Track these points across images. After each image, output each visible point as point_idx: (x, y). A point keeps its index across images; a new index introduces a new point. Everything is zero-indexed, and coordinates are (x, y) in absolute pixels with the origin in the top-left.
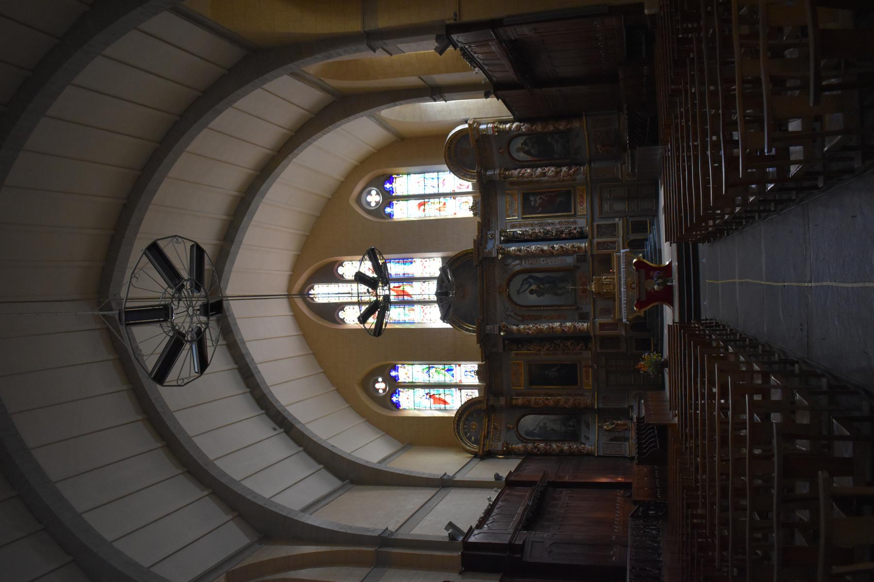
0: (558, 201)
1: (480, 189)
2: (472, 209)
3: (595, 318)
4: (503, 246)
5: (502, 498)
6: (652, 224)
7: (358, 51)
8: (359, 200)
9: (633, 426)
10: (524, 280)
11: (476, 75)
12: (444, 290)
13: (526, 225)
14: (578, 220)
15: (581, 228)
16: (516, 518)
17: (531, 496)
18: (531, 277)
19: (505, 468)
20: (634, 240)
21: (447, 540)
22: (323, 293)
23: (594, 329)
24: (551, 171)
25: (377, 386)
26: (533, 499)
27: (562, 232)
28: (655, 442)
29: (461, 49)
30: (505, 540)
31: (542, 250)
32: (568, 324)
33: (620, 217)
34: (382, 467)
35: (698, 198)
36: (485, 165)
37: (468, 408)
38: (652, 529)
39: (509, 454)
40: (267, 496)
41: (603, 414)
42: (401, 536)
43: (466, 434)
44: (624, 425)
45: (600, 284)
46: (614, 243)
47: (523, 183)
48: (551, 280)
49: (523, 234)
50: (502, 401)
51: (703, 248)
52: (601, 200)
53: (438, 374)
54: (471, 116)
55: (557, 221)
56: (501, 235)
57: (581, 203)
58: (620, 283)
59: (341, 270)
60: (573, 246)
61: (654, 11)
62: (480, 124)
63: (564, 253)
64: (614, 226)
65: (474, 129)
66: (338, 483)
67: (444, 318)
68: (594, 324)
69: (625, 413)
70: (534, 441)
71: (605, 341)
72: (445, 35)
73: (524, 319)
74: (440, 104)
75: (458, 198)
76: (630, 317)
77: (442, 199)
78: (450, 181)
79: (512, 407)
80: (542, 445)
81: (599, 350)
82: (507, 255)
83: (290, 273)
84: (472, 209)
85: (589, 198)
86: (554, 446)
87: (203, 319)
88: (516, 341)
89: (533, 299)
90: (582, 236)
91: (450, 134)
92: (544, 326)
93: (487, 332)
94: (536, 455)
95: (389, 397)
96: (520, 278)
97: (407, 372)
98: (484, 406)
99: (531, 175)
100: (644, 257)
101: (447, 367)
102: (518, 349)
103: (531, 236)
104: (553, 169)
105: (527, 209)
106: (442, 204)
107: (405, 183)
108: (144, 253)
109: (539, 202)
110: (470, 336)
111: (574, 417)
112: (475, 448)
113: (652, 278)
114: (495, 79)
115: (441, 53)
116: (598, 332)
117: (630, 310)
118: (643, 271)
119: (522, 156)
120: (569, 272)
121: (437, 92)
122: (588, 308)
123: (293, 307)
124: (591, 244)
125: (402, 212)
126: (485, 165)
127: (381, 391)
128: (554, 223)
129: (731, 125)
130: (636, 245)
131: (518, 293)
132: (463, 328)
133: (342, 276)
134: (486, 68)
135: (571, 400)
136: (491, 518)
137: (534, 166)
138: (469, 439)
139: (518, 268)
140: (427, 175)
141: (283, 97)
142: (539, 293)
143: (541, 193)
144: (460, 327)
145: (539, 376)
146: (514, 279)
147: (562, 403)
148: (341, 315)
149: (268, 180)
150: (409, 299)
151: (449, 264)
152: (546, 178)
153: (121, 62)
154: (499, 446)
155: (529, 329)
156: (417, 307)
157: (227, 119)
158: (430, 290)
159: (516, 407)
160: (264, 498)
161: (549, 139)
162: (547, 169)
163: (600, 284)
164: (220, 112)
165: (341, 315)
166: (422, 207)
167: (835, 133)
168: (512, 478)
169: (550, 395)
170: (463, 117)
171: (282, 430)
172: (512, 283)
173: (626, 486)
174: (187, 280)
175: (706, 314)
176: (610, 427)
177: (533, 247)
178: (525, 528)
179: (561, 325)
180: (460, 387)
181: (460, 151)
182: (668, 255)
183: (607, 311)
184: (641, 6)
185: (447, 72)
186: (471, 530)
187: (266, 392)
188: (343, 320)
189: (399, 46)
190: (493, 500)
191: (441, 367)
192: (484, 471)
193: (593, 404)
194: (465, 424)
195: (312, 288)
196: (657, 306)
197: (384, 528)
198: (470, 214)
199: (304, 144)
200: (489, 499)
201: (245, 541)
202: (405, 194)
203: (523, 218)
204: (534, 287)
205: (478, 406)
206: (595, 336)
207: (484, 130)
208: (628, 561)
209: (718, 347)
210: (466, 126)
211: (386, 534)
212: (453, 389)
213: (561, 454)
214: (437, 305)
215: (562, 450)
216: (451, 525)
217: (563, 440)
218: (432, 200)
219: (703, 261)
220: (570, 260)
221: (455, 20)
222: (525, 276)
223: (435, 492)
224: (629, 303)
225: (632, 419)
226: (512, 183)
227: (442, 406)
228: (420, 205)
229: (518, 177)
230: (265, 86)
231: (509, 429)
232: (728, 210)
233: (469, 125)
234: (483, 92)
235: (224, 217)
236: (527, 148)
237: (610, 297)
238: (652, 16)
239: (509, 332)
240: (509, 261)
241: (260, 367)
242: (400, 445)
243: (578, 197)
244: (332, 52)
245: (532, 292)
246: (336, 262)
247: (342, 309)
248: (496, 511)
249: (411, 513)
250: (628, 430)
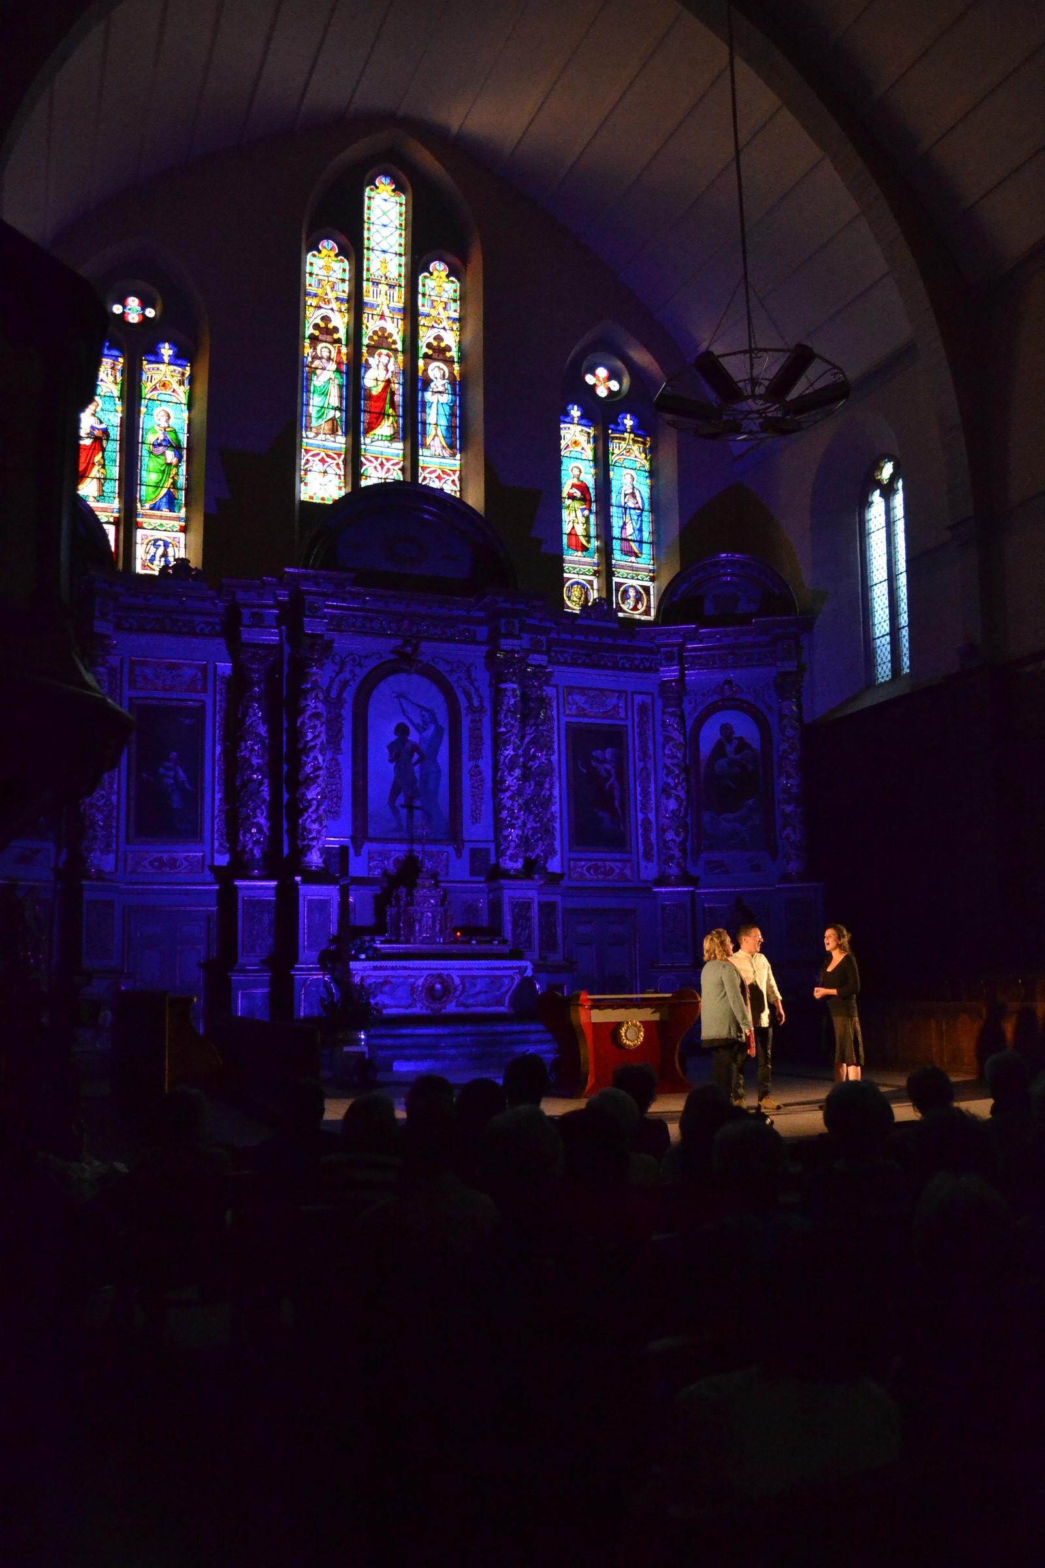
10: (431, 713)
18: (439, 732)
22: (385, 211)
25: (133, 302)
59: (439, 268)
89: (382, 736)
119: (710, 735)
131: (400, 696)
146: (435, 689)
156: (340, 442)
161: (750, 802)
166: (578, 494)
167: (415, 764)
180: (128, 522)
191: (182, 481)
195: (399, 189)
204: (414, 736)
228: (583, 488)
236: (729, 749)
245: (402, 730)
247: (343, 252)
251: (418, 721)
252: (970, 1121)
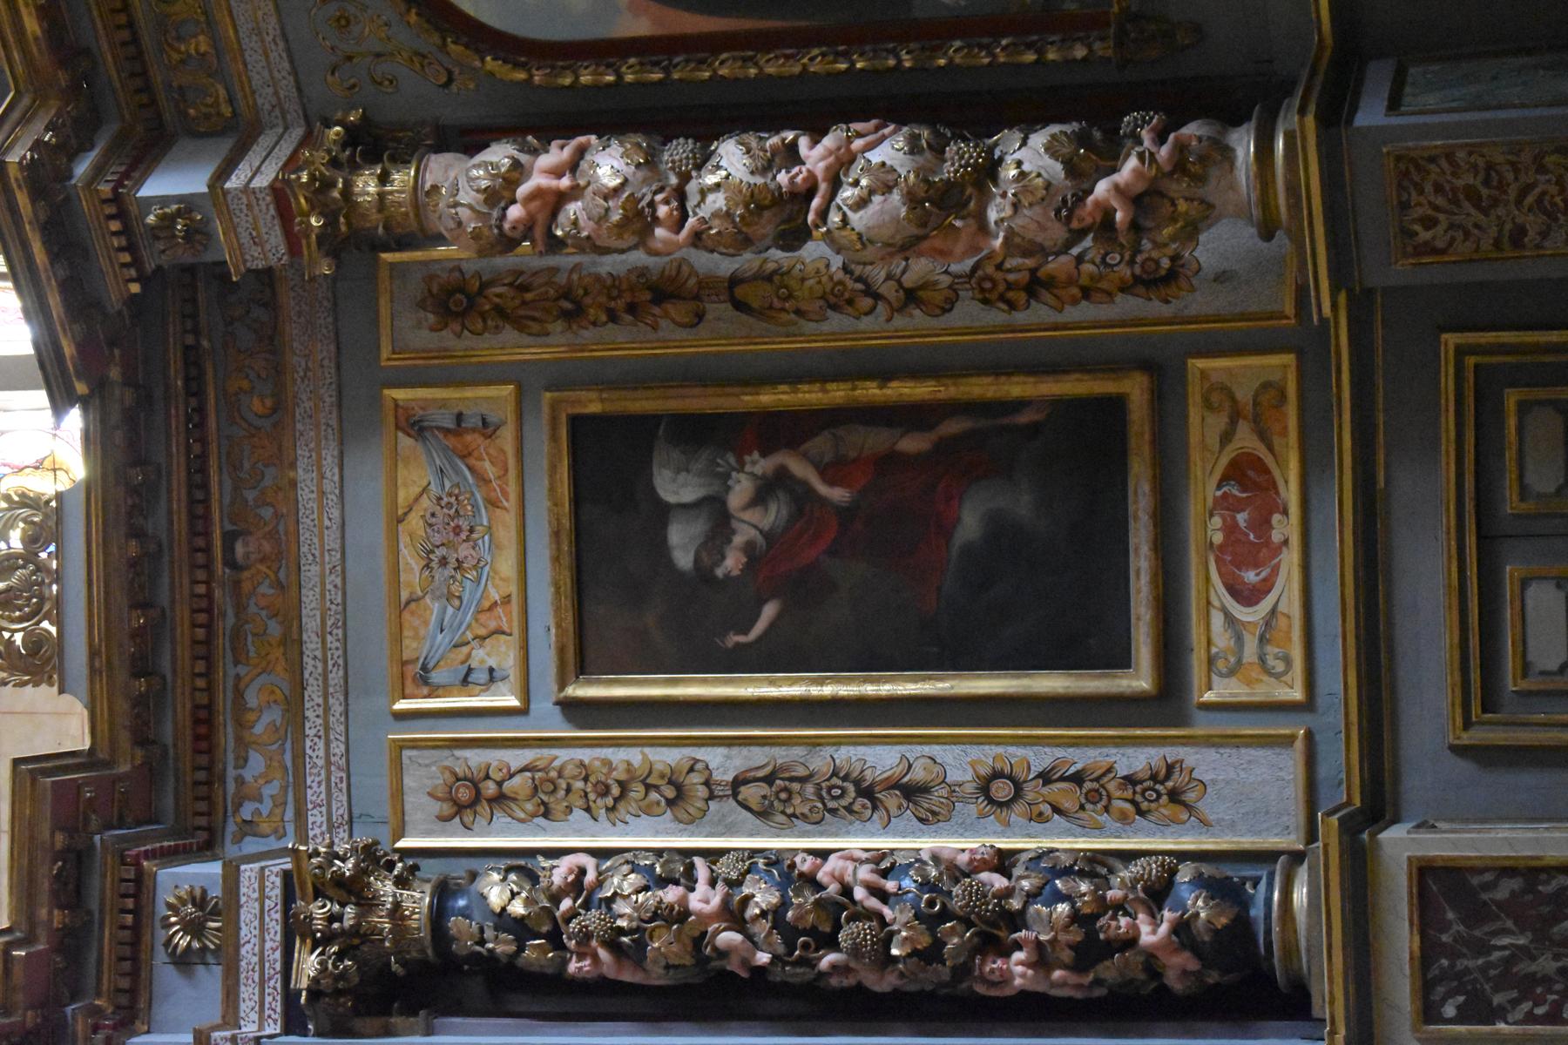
0: (970, 523)
14: (1202, 763)
24: (871, 172)
27: (997, 928)
47: (571, 304)
52: (1488, 537)
55: (958, 759)
56: (294, 930)
57: (1246, 554)
84: (58, 377)
99: (639, 221)
104: (889, 149)
105: (623, 596)
109: (753, 523)
137: (670, 112)
143: (779, 430)
162: (815, 156)
203: (576, 711)
220: (1342, 298)
226: (456, 301)
243: (1204, 484)
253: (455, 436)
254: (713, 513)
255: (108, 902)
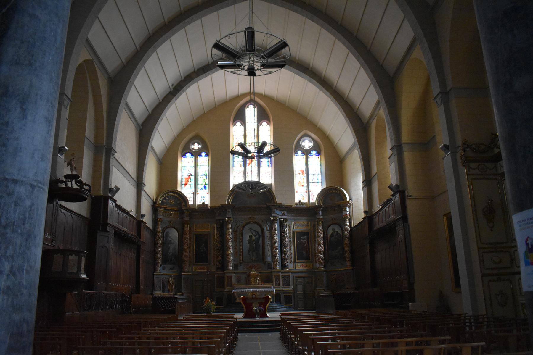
0: (304, 252)
1: (311, 207)
2: (300, 202)
3: (235, 273)
4: (278, 220)
5: (131, 219)
6: (290, 307)
7: (391, 140)
8: (306, 135)
9: (172, 294)
10: (258, 232)
11: (377, 207)
12: (254, 187)
13: (290, 233)
14: (292, 264)
15: (288, 265)
16: (120, 227)
17: (134, 235)
18: (259, 236)
19: (148, 220)
20: (280, 298)
21: (110, 187)
22: (251, 112)
23: (229, 273)
25: (196, 144)
26: (132, 237)
27: (285, 255)
28: (166, 308)
29: (391, 199)
30: (110, 221)
31: (275, 243)
32: (232, 258)
33: (294, 288)
34: (149, 148)
35: (304, 327)
36: (325, 210)
37: (182, 198)
38: (116, 306)
39: (155, 221)
40: (135, 83)
41: (178, 278)
42: (112, 161)
43: (167, 197)
44: (172, 290)
45: (255, 276)
46: (279, 285)
48: (257, 248)
49: (285, 231)
50: (187, 219)
51: (278, 334)
53: (203, 181)
54: (353, 202)
55: (292, 251)
56: (284, 219)
57: (303, 266)
58: (256, 288)
59: (264, 124)
60: (277, 261)
61: (410, 308)
62: (349, 207)
63: (274, 256)
64: (289, 285)
65: (347, 204)
66: (140, 122)
67: (237, 186)
68: (232, 273)
69: (179, 290)
70: (163, 237)
71: (221, 280)
72: (399, 190)
73: (235, 232)
74: (361, 185)
75: (307, 194)
76: (235, 294)
77: (306, 184)
78: (317, 187)
79: (183, 225)
80: (161, 242)
81: (216, 275)
82: (272, 222)
83: (263, 94)
85: (304, 270)
86: (160, 249)
87: (246, 68)
88: (222, 227)
89: (246, 238)
90: (283, 266)
91: (343, 190)
92: (231, 244)
93: (228, 210)
94: (155, 238)
95: (189, 151)
96: (258, 229)
97: (204, 161)
98: (184, 208)
99: (319, 237)
100: (271, 302)
101: (207, 186)
102: (217, 228)
103: (284, 236)
105: (300, 234)
106: (303, 184)
107: (316, 163)
108: (282, 40)
109: (303, 241)
110: (226, 200)
111: (176, 260)
112: (159, 202)
113: (260, 306)
114: (374, 217)
115: (389, 187)
116: (227, 275)
117: (240, 294)
118: (263, 301)
119: (330, 231)
120: (263, 259)
121: (368, 183)
122: (241, 269)
123: (244, 95)
124: (279, 271)
125: (298, 160)
126: (325, 210)
127: (193, 147)
128: (291, 250)
129: (342, 339)
130: (277, 297)
131: (250, 229)
132: (230, 196)
133: (261, 124)
134: (381, 212)
135: (187, 259)
136: (120, 212)
137: (324, 238)
138: (164, 199)
139: (265, 229)
140: (320, 176)
141: (365, 94)
142: (250, 241)
144: (231, 194)
145: (201, 240)
147: (185, 253)
148: (239, 124)
149: (318, 84)
150: (248, 164)
151: (268, 187)
152: (317, 245)
153: (385, 10)
154: (160, 216)
155: (229, 235)
157: (354, 63)
158: (252, 177)
159: (183, 226)
160: (134, 80)
162: (322, 246)
163: (255, 276)
164: (358, 60)
165: (239, 124)
166: (301, 173)
168: (142, 224)
169: (190, 247)
170: (353, 198)
171: (172, 90)
172: (256, 225)
173: (137, 290)
174: (267, 61)
175: (240, 336)
176: (171, 282)
177: (277, 238)
178: (116, 232)
179: (231, 253)
180: (195, 194)
181: (333, 197)
182: (273, 316)
183: (239, 281)
184: (413, 301)
185: (379, 190)
186: (115, 201)
187: (195, 80)
188: (235, 125)
189: (394, 163)
190: (131, 213)
191: (207, 183)
192: (146, 208)
193: (184, 272)
194: (173, 196)
196: (243, 310)
197: (116, 150)
198: (297, 201)
199: (339, 106)
200: (131, 211)
201: (110, 70)
202: (309, 163)
204: (253, 238)
205: (184, 204)
206: (225, 273)
207: (346, 210)
208: (99, 292)
209: (227, 340)
210: (348, 199)
211: (113, 152)
212: (193, 190)
213: (155, 253)
214: (243, 181)
215: (158, 254)
216: (118, 189)
217: (163, 254)
218: (305, 178)
219: (270, 334)
220: (269, 259)
221: (408, 196)
222: (260, 233)
223: (135, 179)
224: (243, 293)
225: (176, 294)
226: (314, 226)
227: (184, 183)
228: (303, 172)
229: (318, 229)
230: (372, 86)
231: (170, 222)
232: (300, 343)
233: (349, 201)
234: (367, 210)
235: (297, 58)
236: (335, 234)
237: (247, 283)
238: (408, 306)
239: (227, 223)
240: (269, 224)
241: (209, 77)
242: (161, 158)
244: (391, 125)
245: (251, 236)
246: (270, 121)
247: (242, 125)
248: (125, 215)
249: (123, 165)
250: (169, 292)
251: (254, 234)
252: (83, 279)
253: (307, 225)
254: (304, 239)
255: (339, 317)
